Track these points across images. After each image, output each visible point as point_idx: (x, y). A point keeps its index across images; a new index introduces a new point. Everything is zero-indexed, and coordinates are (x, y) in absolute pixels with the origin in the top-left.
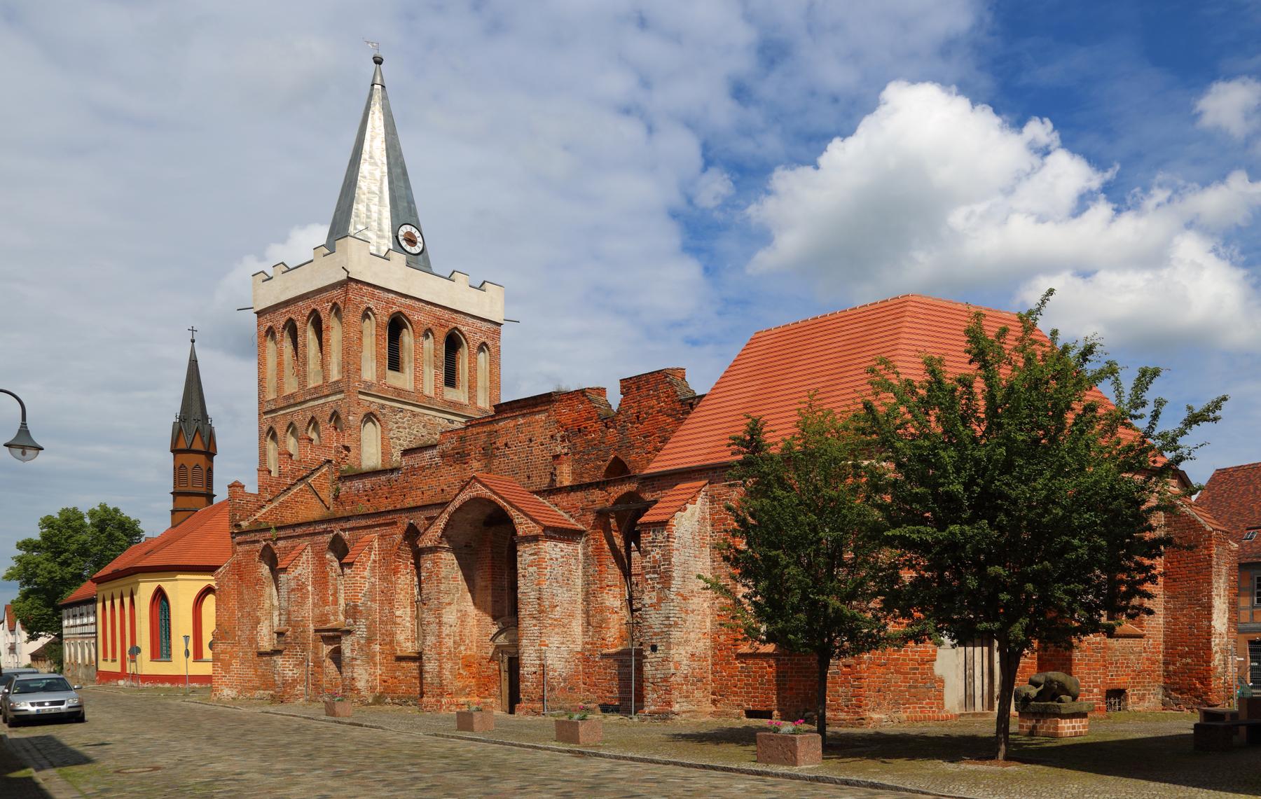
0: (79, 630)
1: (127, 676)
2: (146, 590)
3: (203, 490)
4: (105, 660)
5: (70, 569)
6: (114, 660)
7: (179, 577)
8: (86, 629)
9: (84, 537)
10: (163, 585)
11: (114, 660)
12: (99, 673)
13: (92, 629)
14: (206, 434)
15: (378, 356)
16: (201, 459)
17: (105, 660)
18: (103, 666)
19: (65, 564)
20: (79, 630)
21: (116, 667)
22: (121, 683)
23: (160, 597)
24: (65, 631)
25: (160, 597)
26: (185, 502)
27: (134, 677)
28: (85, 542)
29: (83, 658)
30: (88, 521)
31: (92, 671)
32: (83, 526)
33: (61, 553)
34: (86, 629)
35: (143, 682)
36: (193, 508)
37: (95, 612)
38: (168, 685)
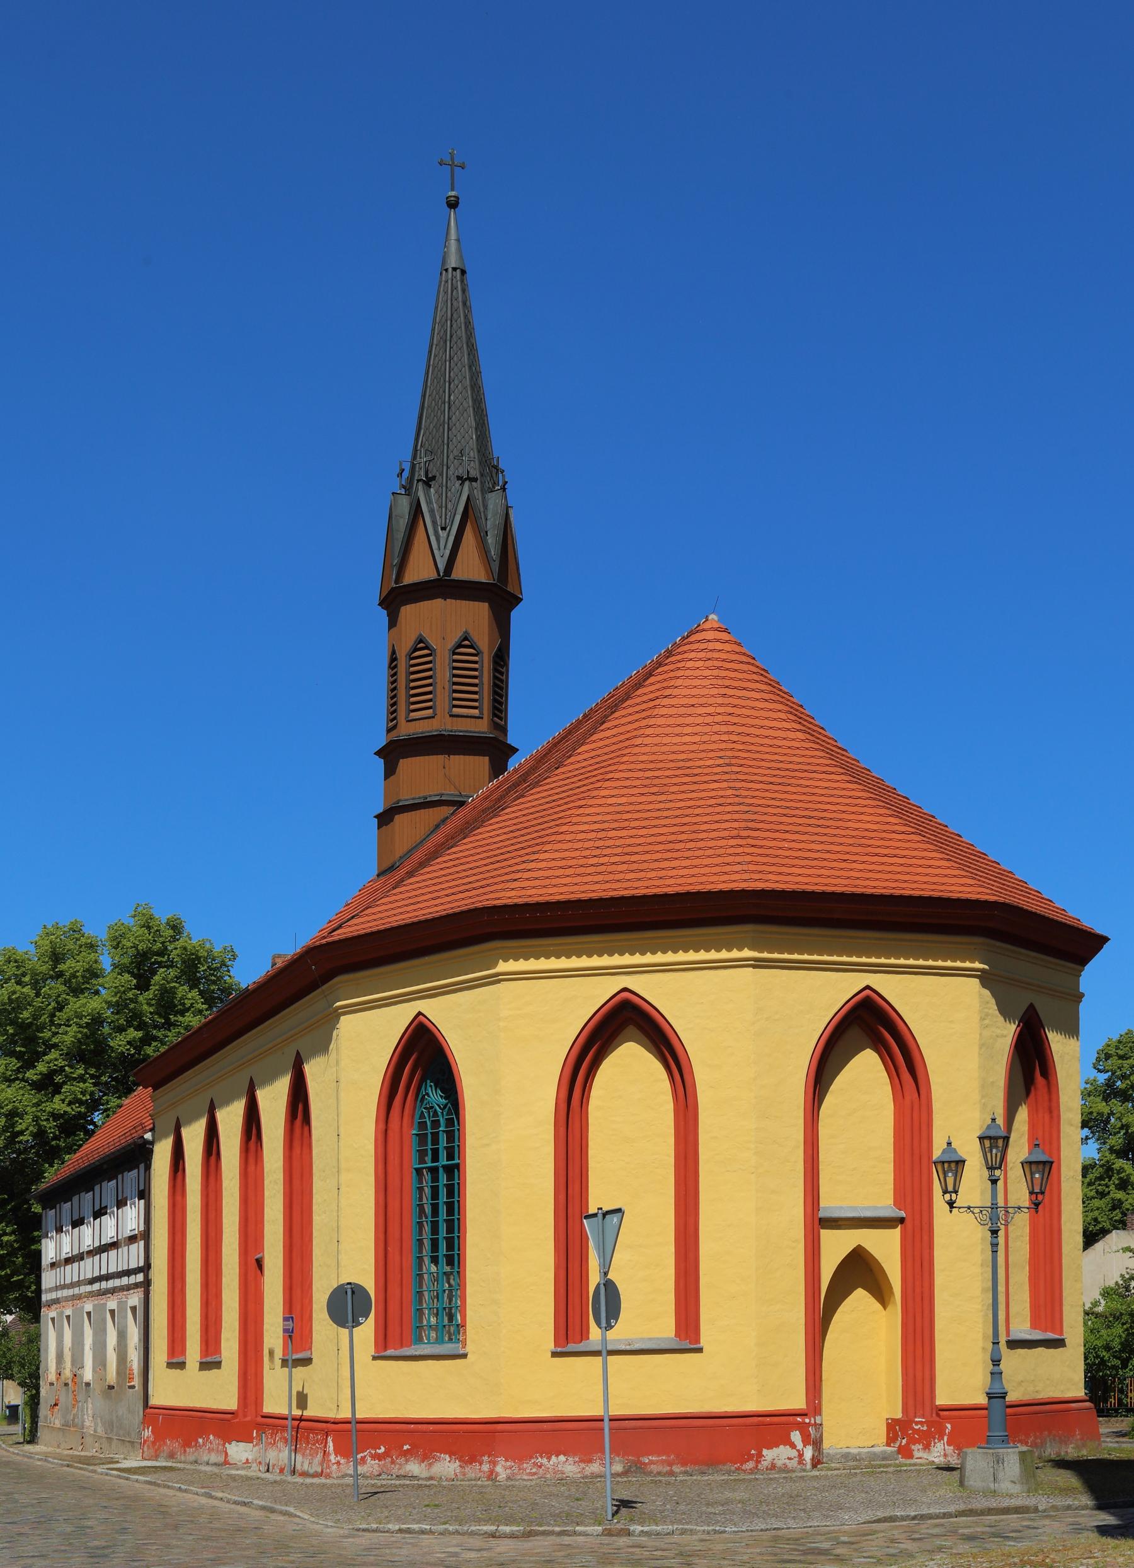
0: (89, 1268)
1: (272, 1424)
2: (362, 1042)
3: (482, 727)
4: (176, 1364)
5: (58, 1104)
6: (210, 1364)
7: (503, 967)
8: (113, 1262)
9: (94, 1004)
10: (429, 1007)
11: (210, 1364)
12: (152, 1414)
13: (133, 1256)
14: (492, 524)
15: (47, 1350)
16: (474, 617)
17: (176, 1364)
18: (172, 1389)
19: (48, 1085)
20: (89, 1268)
21: (219, 1391)
22: (239, 1451)
23: (423, 1062)
24: (49, 1279)
25: (423, 1062)
26: (424, 775)
27: (303, 1429)
28: (97, 1021)
29: (100, 1362)
30: (106, 961)
31: (130, 1411)
32: (93, 973)
33: (36, 1057)
34: (113, 1262)
35: (427, 1456)
36: (450, 793)
37: (144, 1194)
38: (446, 1467)
